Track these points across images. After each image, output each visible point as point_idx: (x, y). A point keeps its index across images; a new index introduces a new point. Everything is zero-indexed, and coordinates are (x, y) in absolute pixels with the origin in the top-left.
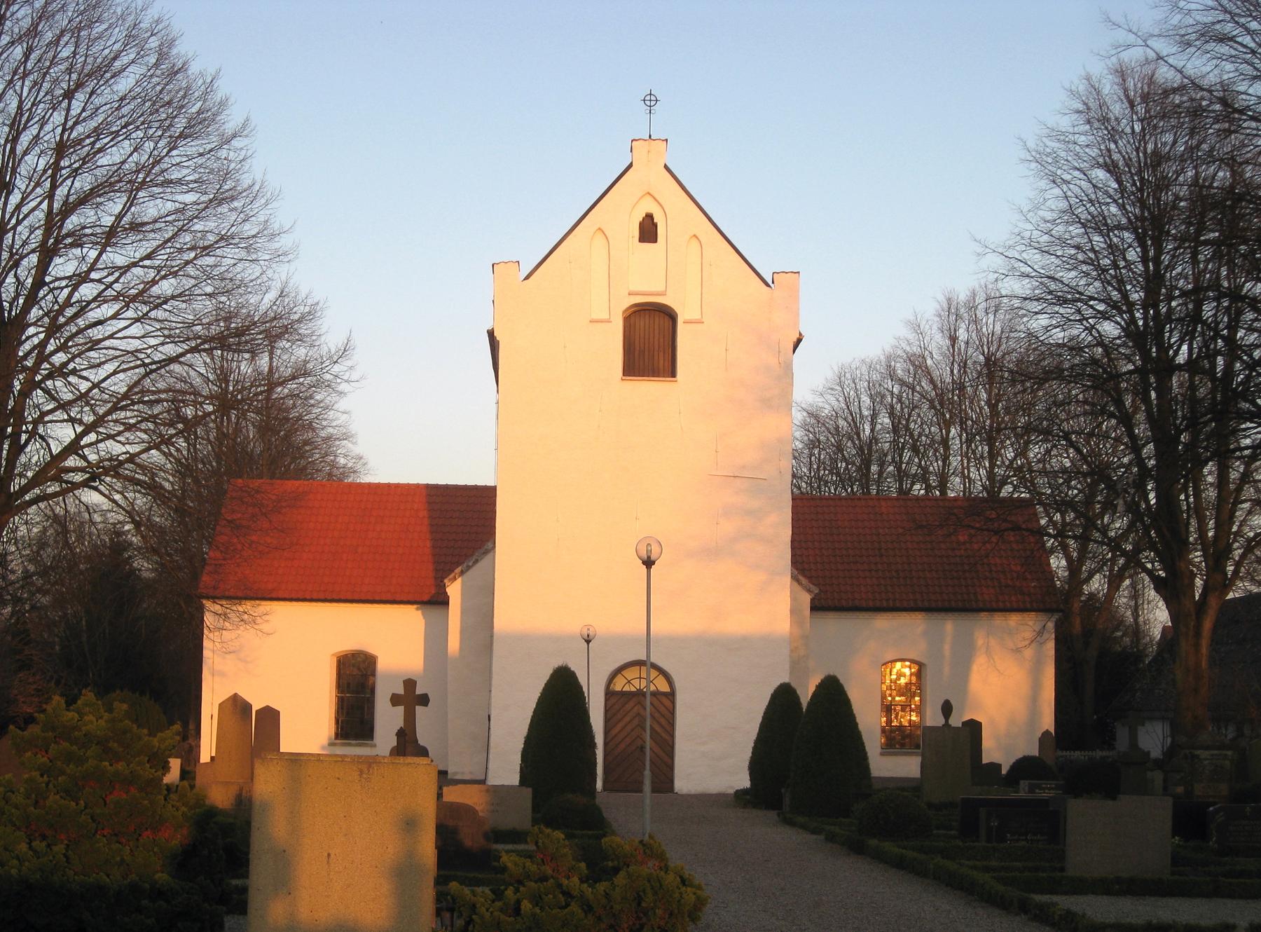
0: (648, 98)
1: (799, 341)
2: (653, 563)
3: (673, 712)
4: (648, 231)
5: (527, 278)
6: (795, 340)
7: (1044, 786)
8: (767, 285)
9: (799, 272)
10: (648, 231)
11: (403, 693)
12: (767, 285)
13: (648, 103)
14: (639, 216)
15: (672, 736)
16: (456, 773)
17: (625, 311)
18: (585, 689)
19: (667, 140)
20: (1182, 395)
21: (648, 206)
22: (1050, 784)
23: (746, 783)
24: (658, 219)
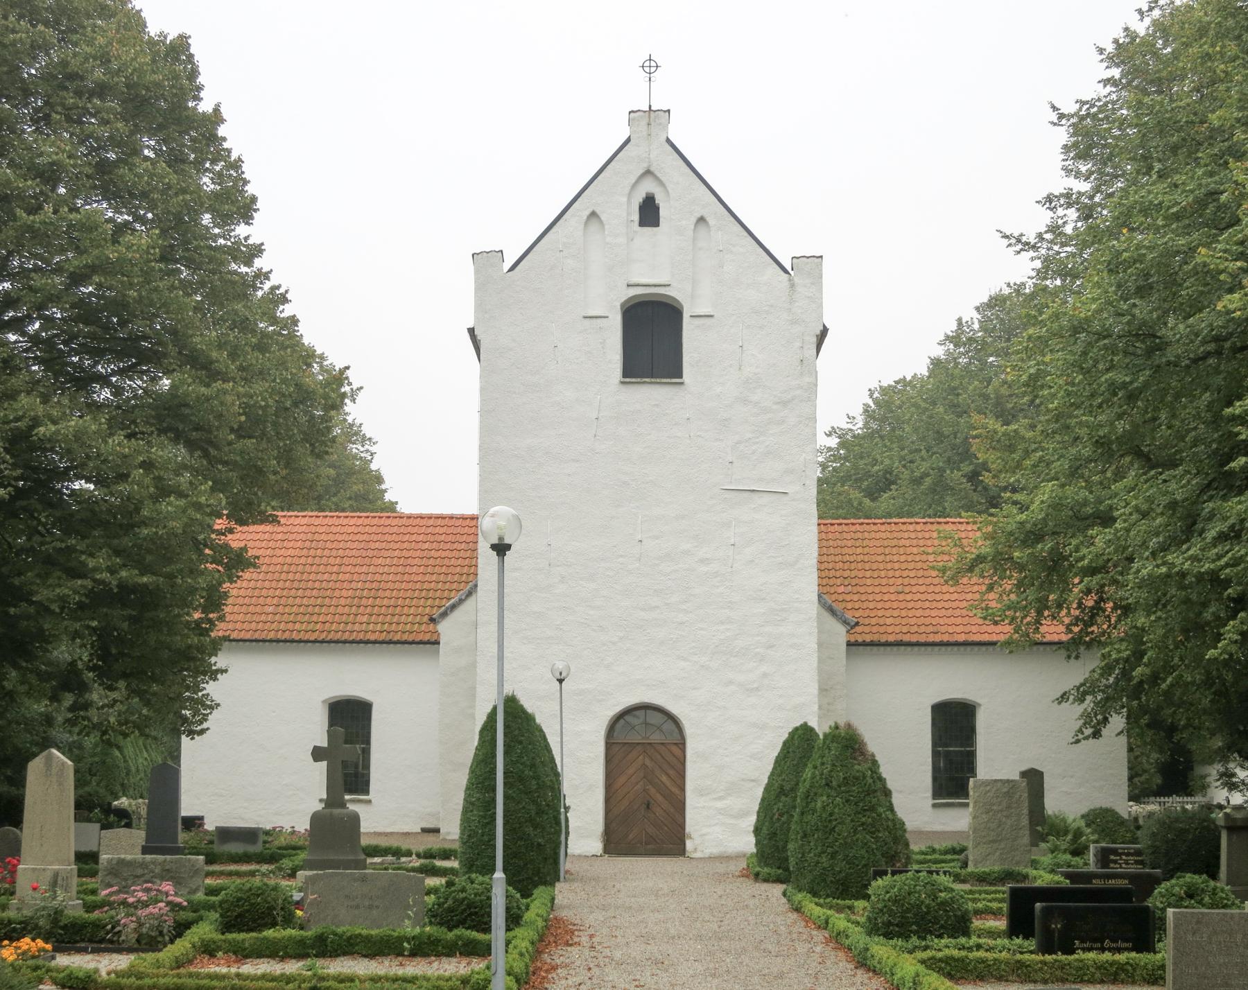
0: (647, 64)
1: (824, 332)
2: (508, 547)
3: (683, 763)
4: (649, 213)
5: (512, 269)
6: (818, 333)
7: (1120, 851)
8: (786, 271)
9: (821, 257)
10: (649, 213)
11: (325, 745)
12: (786, 271)
13: (647, 69)
14: (639, 197)
15: (682, 789)
16: (448, 833)
17: (622, 305)
18: (553, 741)
19: (669, 111)
20: (1144, 599)
21: (648, 187)
22: (1128, 849)
23: (755, 850)
24: (659, 199)
